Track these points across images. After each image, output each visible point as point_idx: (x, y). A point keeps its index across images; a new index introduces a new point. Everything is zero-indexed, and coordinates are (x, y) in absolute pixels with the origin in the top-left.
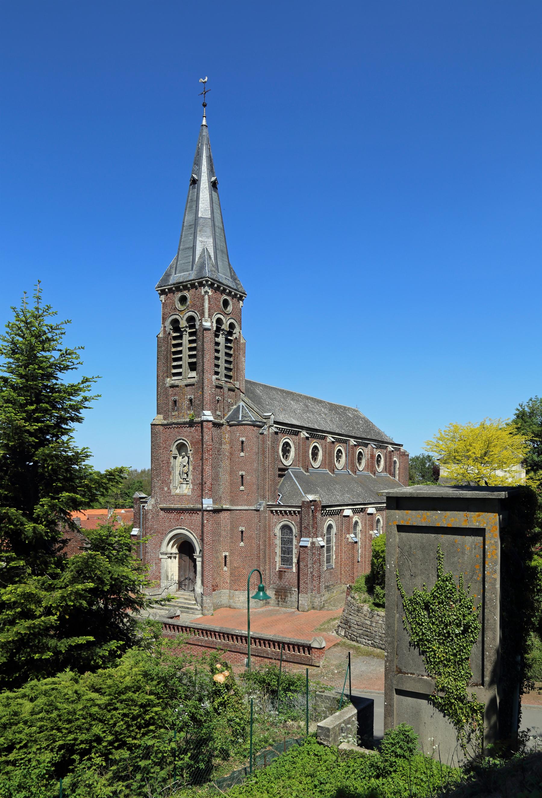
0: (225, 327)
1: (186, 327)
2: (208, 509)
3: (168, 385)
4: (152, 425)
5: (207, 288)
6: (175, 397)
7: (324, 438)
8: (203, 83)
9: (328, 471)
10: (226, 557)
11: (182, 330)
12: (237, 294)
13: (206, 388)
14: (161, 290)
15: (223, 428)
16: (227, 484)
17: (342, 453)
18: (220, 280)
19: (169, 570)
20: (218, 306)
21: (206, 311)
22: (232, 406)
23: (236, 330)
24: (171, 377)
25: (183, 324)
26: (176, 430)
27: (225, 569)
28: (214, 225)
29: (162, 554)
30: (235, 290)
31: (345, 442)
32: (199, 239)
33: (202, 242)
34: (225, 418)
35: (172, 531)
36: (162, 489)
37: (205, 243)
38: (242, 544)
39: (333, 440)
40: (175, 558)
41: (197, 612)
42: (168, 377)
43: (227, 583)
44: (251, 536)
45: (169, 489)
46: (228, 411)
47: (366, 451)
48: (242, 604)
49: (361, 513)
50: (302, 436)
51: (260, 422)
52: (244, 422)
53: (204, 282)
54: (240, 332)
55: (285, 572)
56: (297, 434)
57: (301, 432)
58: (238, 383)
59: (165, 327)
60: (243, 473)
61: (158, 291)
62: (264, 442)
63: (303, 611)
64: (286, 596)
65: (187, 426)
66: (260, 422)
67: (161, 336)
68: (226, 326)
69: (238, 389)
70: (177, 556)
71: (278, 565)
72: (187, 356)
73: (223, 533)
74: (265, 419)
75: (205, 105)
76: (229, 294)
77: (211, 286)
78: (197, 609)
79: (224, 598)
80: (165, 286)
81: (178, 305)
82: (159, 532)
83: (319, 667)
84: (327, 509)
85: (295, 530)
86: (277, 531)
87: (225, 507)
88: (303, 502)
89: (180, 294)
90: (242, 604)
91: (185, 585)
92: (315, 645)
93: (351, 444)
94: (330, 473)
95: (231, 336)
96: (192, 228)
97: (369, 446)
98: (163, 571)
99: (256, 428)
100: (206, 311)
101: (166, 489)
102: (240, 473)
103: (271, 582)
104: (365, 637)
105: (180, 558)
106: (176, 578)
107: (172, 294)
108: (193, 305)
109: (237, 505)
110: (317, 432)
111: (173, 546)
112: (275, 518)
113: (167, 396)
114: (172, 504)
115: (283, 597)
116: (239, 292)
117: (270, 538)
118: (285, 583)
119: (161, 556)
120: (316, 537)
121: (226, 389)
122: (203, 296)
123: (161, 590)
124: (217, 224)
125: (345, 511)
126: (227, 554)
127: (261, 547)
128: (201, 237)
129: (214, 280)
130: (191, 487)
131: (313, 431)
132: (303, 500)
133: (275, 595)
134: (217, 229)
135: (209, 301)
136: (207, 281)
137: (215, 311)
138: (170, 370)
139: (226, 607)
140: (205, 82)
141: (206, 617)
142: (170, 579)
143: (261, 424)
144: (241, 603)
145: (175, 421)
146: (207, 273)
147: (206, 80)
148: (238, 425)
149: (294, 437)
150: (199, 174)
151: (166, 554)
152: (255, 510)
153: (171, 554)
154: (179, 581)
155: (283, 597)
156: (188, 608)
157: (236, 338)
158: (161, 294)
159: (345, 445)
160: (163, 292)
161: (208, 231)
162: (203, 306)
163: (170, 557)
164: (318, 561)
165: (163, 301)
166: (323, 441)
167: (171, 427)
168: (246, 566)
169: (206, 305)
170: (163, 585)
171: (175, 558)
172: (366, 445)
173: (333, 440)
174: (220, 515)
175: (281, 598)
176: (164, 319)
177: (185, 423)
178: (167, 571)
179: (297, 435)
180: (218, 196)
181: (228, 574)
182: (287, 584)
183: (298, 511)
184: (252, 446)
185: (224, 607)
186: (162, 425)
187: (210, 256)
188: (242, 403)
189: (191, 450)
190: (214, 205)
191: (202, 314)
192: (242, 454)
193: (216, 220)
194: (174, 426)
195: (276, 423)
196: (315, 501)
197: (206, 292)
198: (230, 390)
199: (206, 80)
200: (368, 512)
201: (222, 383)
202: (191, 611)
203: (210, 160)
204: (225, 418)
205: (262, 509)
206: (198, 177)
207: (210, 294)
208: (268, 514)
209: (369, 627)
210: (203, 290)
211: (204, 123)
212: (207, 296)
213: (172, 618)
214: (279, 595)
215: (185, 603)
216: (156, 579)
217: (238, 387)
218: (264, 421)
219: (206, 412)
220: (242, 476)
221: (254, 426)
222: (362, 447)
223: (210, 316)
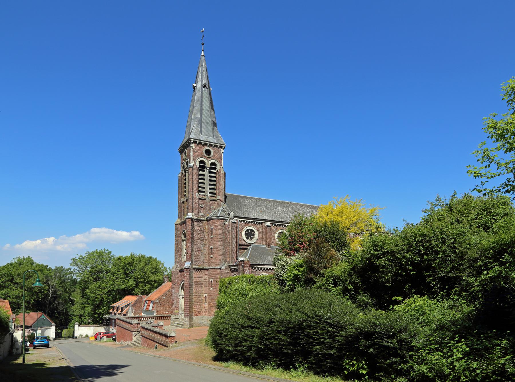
0: (208, 163)
23: (218, 167)
27: (206, 304)
46: (210, 213)
75: (203, 44)
77: (195, 142)
87: (205, 267)
100: (192, 157)
121: (208, 200)
190: (204, 98)
211: (203, 54)
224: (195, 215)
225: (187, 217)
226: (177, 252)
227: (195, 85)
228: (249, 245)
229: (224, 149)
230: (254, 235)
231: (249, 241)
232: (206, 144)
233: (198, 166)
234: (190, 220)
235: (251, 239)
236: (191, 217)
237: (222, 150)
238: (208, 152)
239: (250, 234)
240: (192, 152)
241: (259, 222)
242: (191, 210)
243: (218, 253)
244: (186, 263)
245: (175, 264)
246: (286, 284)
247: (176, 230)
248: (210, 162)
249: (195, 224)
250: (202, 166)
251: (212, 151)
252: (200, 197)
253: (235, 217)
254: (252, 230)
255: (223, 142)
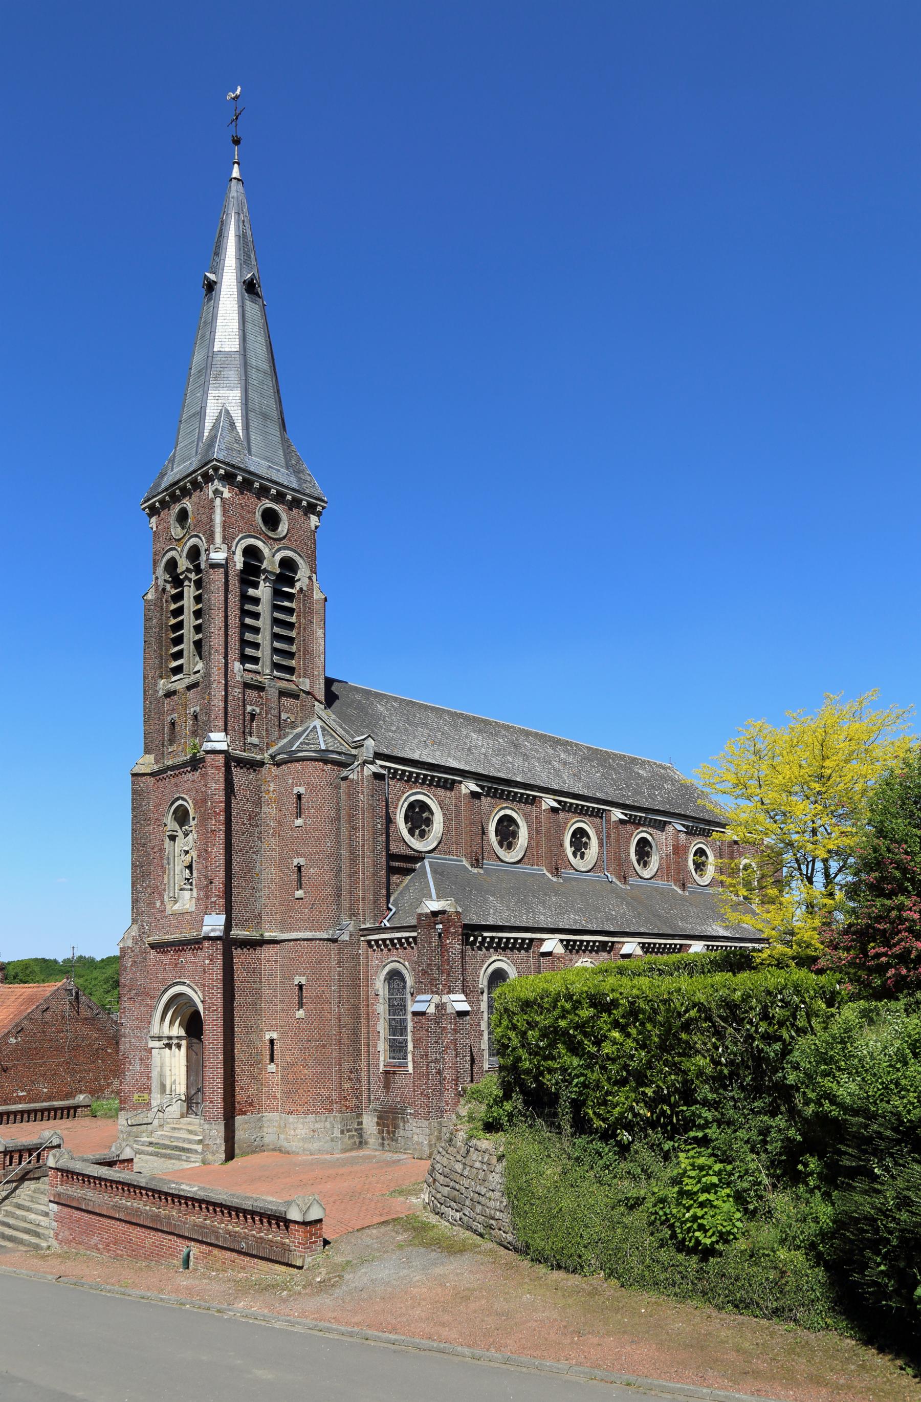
0: (271, 561)
1: (188, 570)
2: (212, 934)
3: (161, 693)
4: (134, 775)
5: (217, 484)
6: (173, 716)
7: (533, 801)
8: (233, 99)
9: (545, 872)
10: (272, 1041)
11: (181, 577)
12: (302, 500)
13: (214, 686)
14: (148, 507)
15: (264, 770)
16: (273, 887)
17: (589, 838)
18: (252, 469)
19: (168, 1073)
20: (250, 523)
21: (218, 530)
22: (294, 728)
23: (303, 573)
24: (168, 677)
25: (183, 564)
26: (173, 780)
27: (272, 1068)
28: (246, 365)
29: (153, 1038)
30: (294, 490)
31: (598, 814)
32: (212, 393)
33: (217, 398)
34: (270, 752)
35: (166, 990)
36: (151, 904)
37: (224, 399)
38: (301, 1013)
39: (556, 805)
40: (179, 1046)
41: (193, 1157)
42: (161, 677)
43: (275, 1097)
44: (319, 997)
45: (162, 903)
46: (280, 738)
47: (662, 841)
48: (301, 1144)
49: (604, 954)
50: (464, 791)
51: (340, 753)
52: (300, 754)
53: (211, 472)
54: (310, 578)
55: (394, 1073)
56: (450, 786)
57: (461, 782)
58: (307, 681)
59: (157, 578)
60: (302, 861)
61: (144, 509)
62: (352, 795)
63: (421, 1159)
64: (396, 1127)
65: (189, 769)
66: (340, 753)
67: (150, 597)
68: (273, 563)
69: (308, 693)
70: (184, 1043)
71: (382, 1058)
72: (192, 629)
73: (266, 991)
74: (355, 748)
75: (237, 142)
76: (280, 497)
77: (229, 478)
78: (196, 1151)
79: (270, 1130)
80: (154, 497)
81: (177, 531)
82: (148, 994)
83: (301, 1268)
84: (485, 934)
85: (410, 981)
86: (380, 985)
87: (268, 935)
88: (420, 915)
89: (176, 508)
90: (301, 1144)
91: (197, 1103)
92: (294, 1214)
93: (614, 819)
94: (549, 876)
95: (292, 586)
96: (201, 375)
97: (669, 828)
98: (155, 1074)
99: (329, 766)
100: (218, 530)
101: (158, 904)
102: (296, 862)
103: (372, 1097)
104: (452, 1204)
105: (189, 1047)
106: (181, 1089)
107: (166, 510)
108: (198, 523)
109: (291, 930)
110: (510, 786)
111: (172, 1023)
112: (375, 958)
113: (161, 714)
114: (167, 933)
115: (391, 1129)
116: (304, 494)
117: (368, 1001)
118: (395, 1098)
119: (152, 1044)
120: (449, 993)
121: (273, 693)
122: (212, 501)
123: (151, 1114)
124: (253, 362)
125: (546, 943)
126: (275, 1035)
127: (345, 1020)
128: (217, 388)
129: (233, 466)
130: (195, 895)
131: (499, 784)
132: (419, 911)
133: (378, 1124)
134: (253, 373)
135: (225, 512)
136: (216, 469)
137: (240, 531)
138: (166, 662)
139: (274, 1150)
140: (237, 97)
141: (208, 1166)
142: (168, 1091)
143: (343, 758)
144: (299, 1141)
145: (170, 763)
146: (218, 453)
147: (238, 92)
148: (291, 762)
149: (441, 792)
150: (217, 268)
151: (160, 1038)
152: (328, 940)
153: (170, 1038)
154: (187, 1096)
155: (391, 1129)
156: (183, 1150)
157: (301, 589)
158: (150, 516)
159: (598, 820)
160: (153, 511)
161: (233, 375)
162: (211, 520)
163: (169, 1046)
164: (452, 1047)
165: (154, 529)
166: (528, 808)
167: (165, 775)
168: (311, 1062)
169: (218, 518)
170: (154, 1103)
171: (179, 1046)
172: (662, 826)
173: (556, 805)
174: (258, 952)
175: (388, 1132)
176: (155, 563)
177: (184, 765)
178: (162, 1075)
179: (451, 789)
180: (265, 315)
181: (278, 1078)
182: (398, 1099)
183: (414, 938)
184: (320, 806)
185: (268, 1150)
186: (152, 774)
187: (232, 425)
188: (318, 723)
189: (194, 818)
190: (249, 326)
191: (211, 538)
192: (299, 822)
193: (250, 354)
194: (169, 773)
195: (378, 755)
196: (443, 912)
197: (216, 492)
198: (282, 693)
199: (238, 92)
200: (623, 952)
201: (265, 680)
202: (184, 1155)
203: (242, 239)
204: (270, 752)
205: (346, 937)
206: (217, 277)
207: (226, 494)
208: (363, 949)
209: (458, 1178)
210: (211, 488)
211: (236, 173)
212: (218, 500)
213: (110, 1164)
214: (384, 1125)
215: (184, 1140)
216: (141, 1090)
217: (307, 688)
218: (354, 752)
219: (213, 736)
220: (299, 868)
221: (326, 762)
222: (650, 830)
223: (226, 539)
224: (233, 741)
225: (208, 746)
226: (143, 878)
227: (212, 277)
228: (418, 857)
229: (319, 515)
230: (429, 822)
231: (417, 844)
232: (263, 492)
233: (239, 566)
234: (221, 759)
235: (422, 835)
236: (223, 746)
237: (314, 520)
238: (271, 519)
239: (418, 817)
240: (218, 512)
241: (442, 778)
242: (221, 724)
243: (325, 885)
244: (208, 919)
245: (134, 921)
246: (740, 1021)
247: (138, 796)
248: (278, 557)
249: (239, 775)
250: (251, 571)
251: (284, 516)
252: (248, 677)
253: (378, 755)
254: (424, 807)
255: (317, 489)
